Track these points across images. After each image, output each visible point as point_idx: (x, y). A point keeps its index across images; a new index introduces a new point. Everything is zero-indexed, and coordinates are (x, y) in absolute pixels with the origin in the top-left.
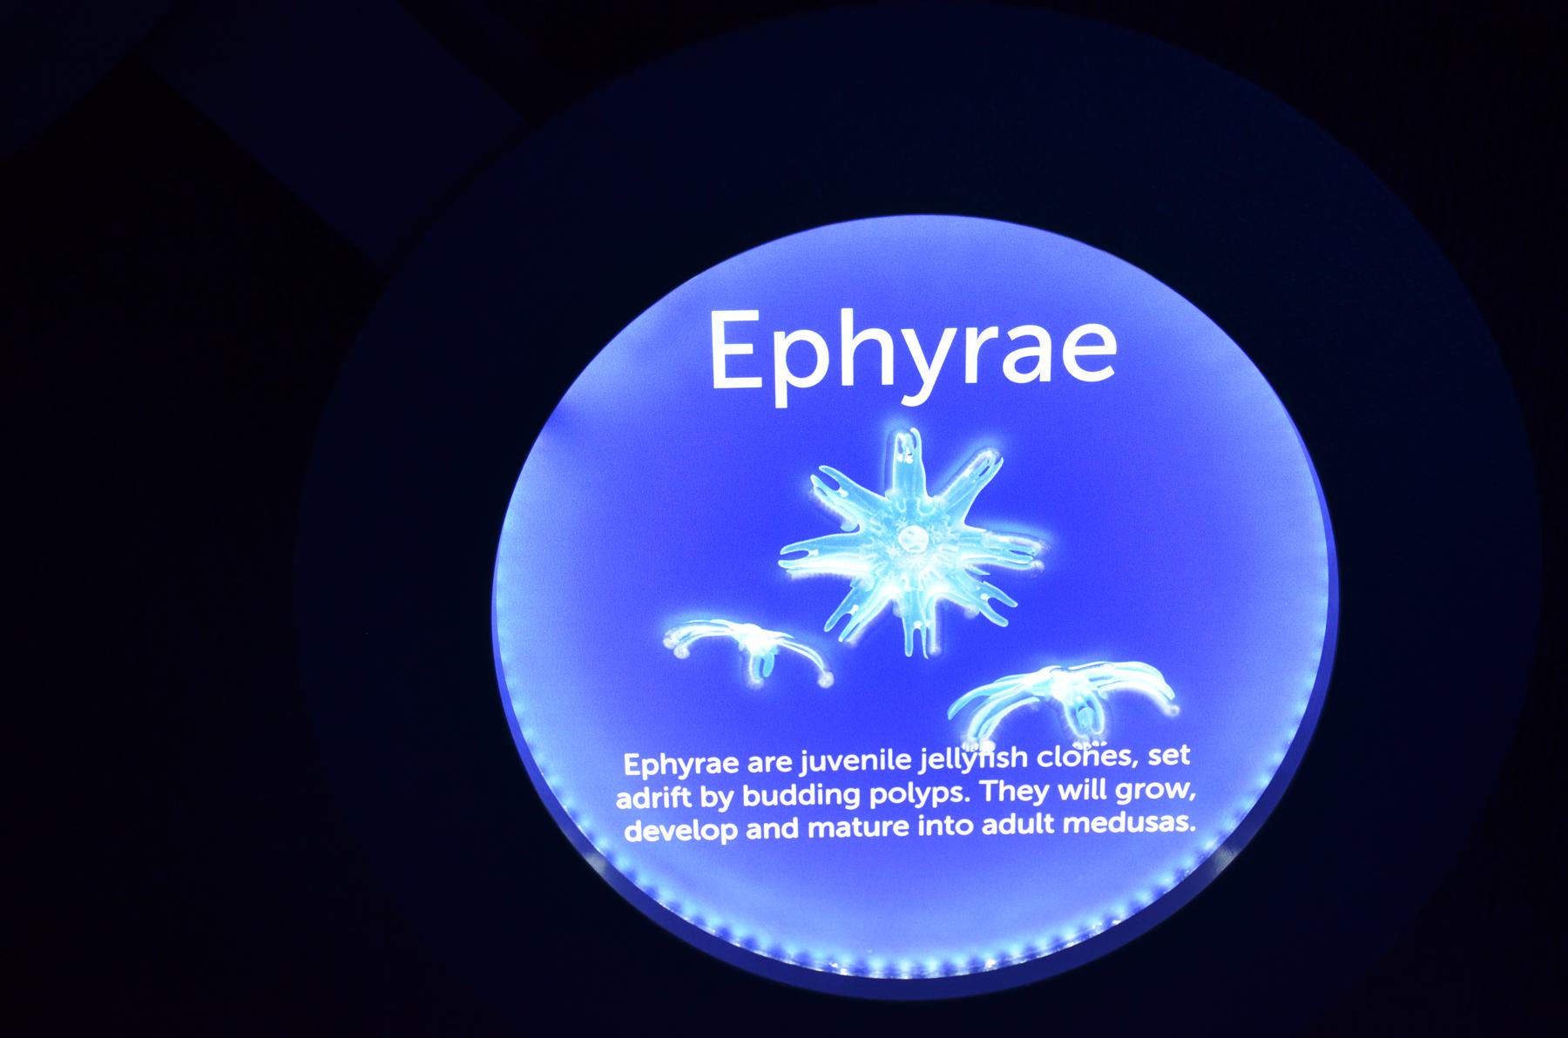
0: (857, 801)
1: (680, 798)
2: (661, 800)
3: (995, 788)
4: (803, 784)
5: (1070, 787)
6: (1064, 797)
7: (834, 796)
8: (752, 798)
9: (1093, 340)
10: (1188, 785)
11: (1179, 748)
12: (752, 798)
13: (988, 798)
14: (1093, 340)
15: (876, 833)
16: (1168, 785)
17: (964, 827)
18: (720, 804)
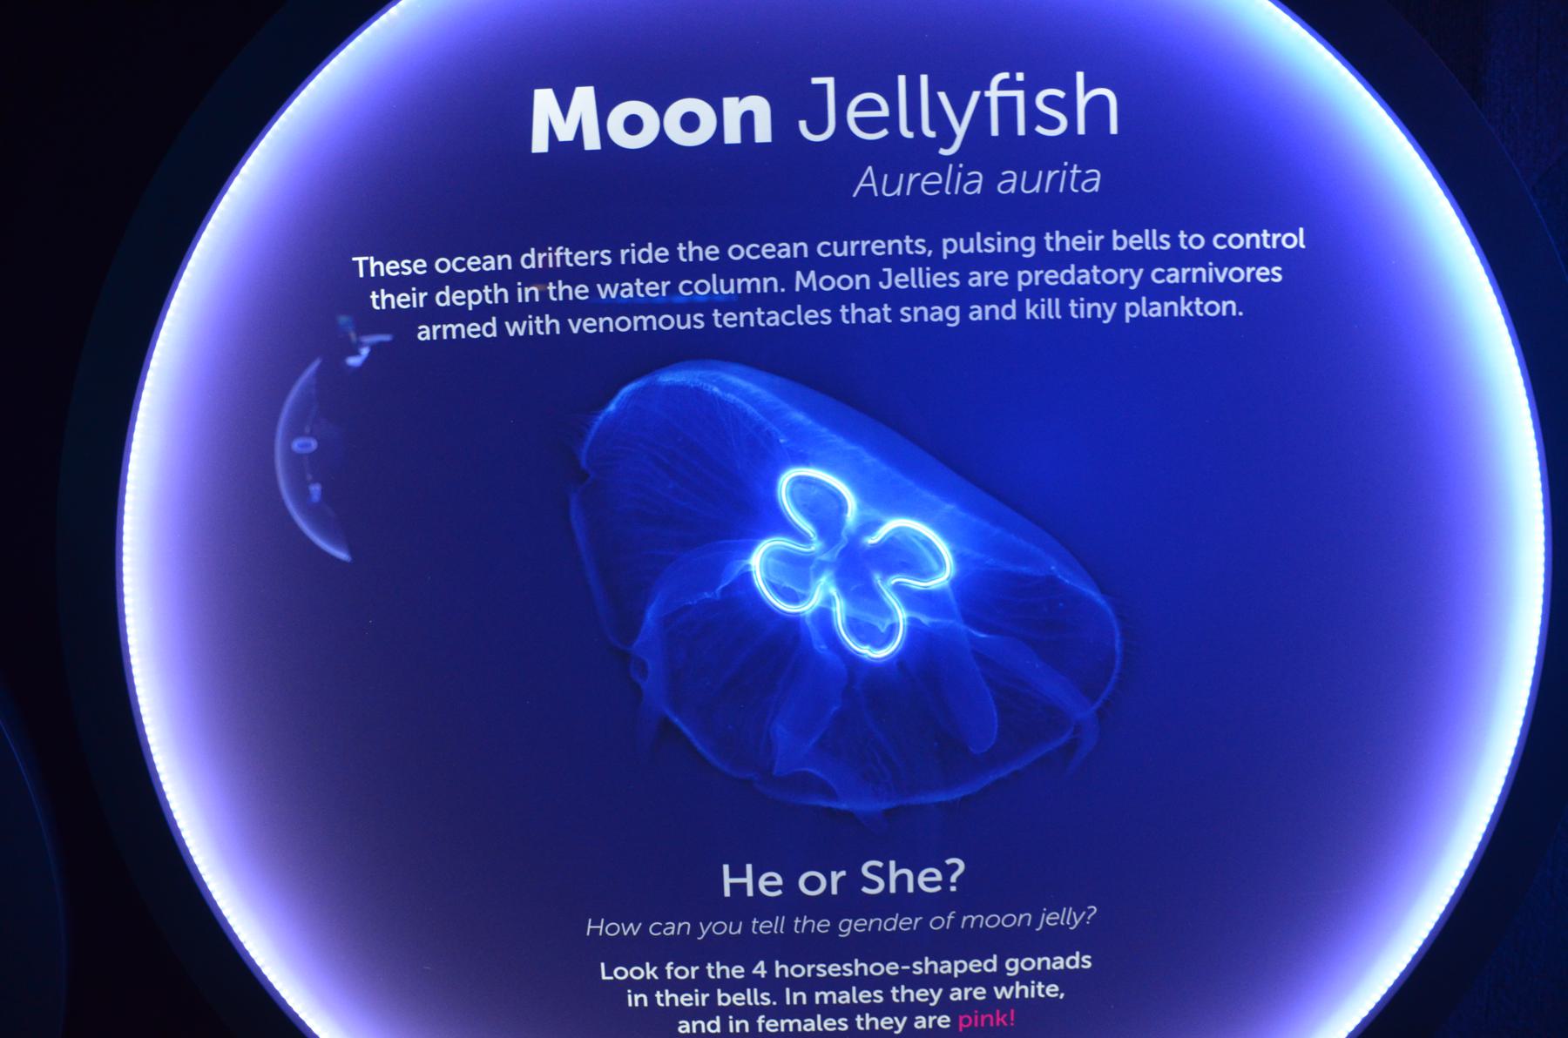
1: (563, 258)
2: (545, 260)
3: (366, 264)
4: (1009, 982)
5: (516, 324)
6: (999, 996)
7: (1011, 244)
9: (772, 879)
10: (540, 144)
12: (1120, 242)
13: (361, 275)
14: (772, 879)
16: (592, 142)
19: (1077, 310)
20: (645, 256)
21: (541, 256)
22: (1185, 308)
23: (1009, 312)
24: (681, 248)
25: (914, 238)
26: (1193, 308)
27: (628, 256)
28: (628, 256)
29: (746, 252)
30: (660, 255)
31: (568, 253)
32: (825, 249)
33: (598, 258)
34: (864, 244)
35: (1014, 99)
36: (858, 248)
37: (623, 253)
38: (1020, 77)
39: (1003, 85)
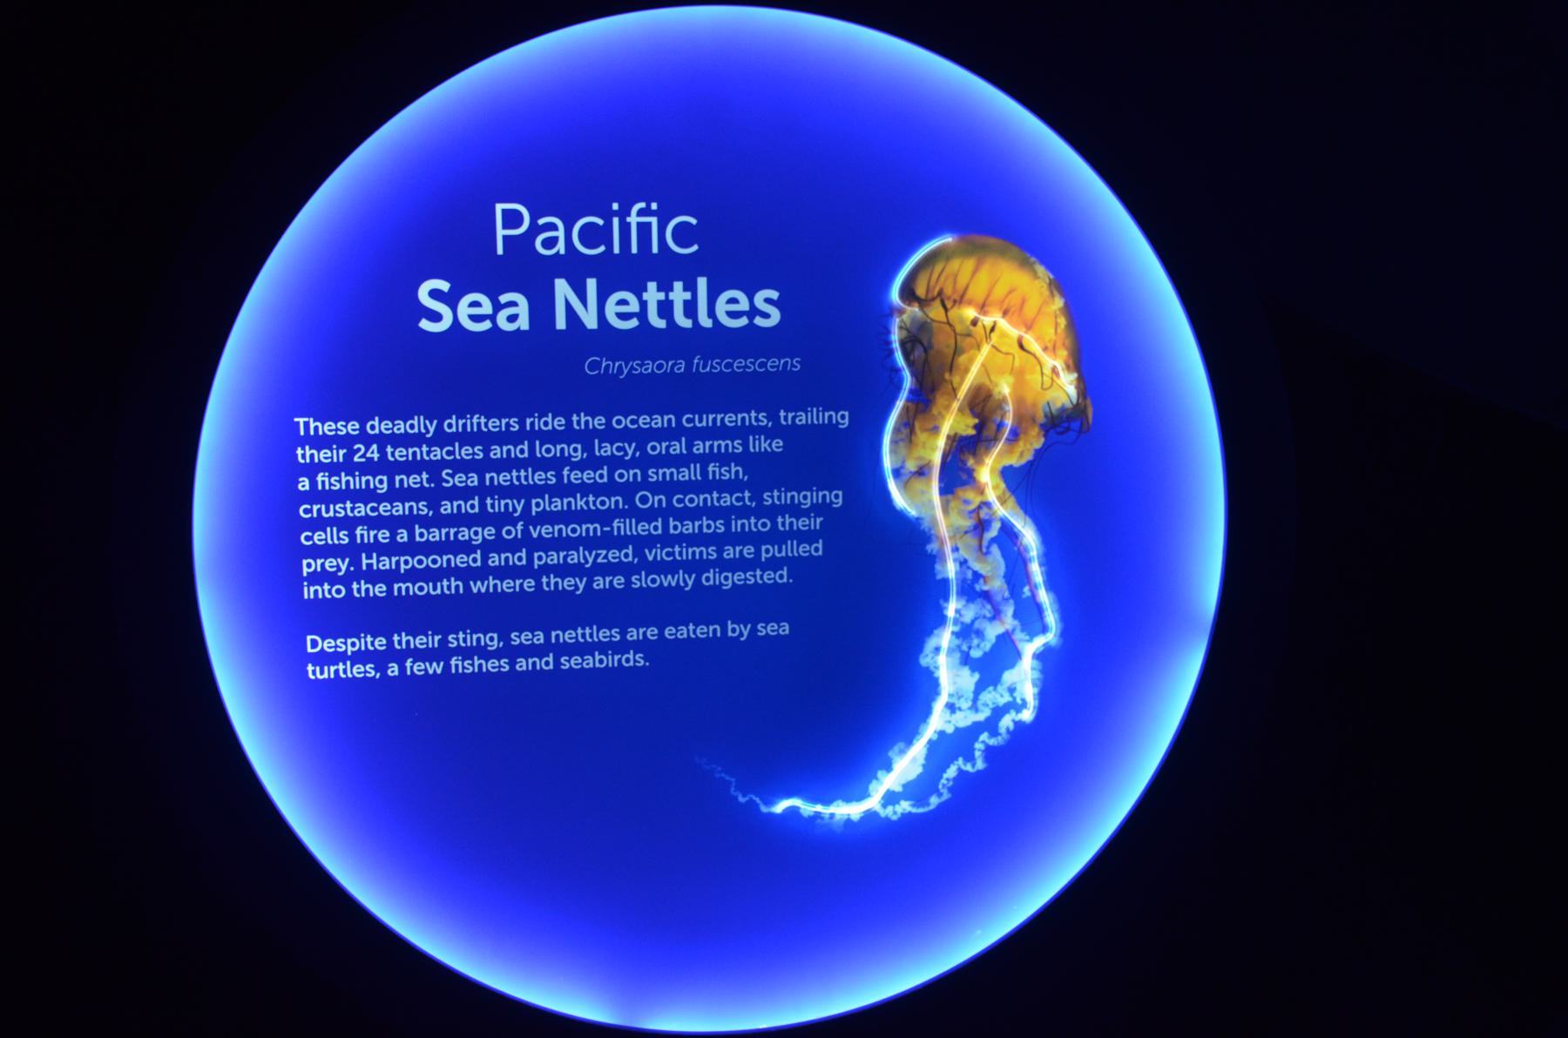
0: (385, 485)
2: (465, 425)
3: (307, 425)
8: (421, 535)
11: (639, 291)
15: (326, 675)
17: (338, 591)
18: (741, 634)
19: (493, 506)
20: (546, 424)
21: (461, 422)
22: (581, 503)
23: (473, 507)
24: (575, 418)
25: (758, 412)
26: (587, 503)
27: (532, 424)
28: (532, 424)
29: (626, 422)
30: (558, 423)
31: (483, 420)
32: (689, 421)
33: (508, 425)
34: (719, 417)
35: (649, 224)
36: (714, 420)
37: (528, 421)
38: (654, 206)
39: (641, 213)
